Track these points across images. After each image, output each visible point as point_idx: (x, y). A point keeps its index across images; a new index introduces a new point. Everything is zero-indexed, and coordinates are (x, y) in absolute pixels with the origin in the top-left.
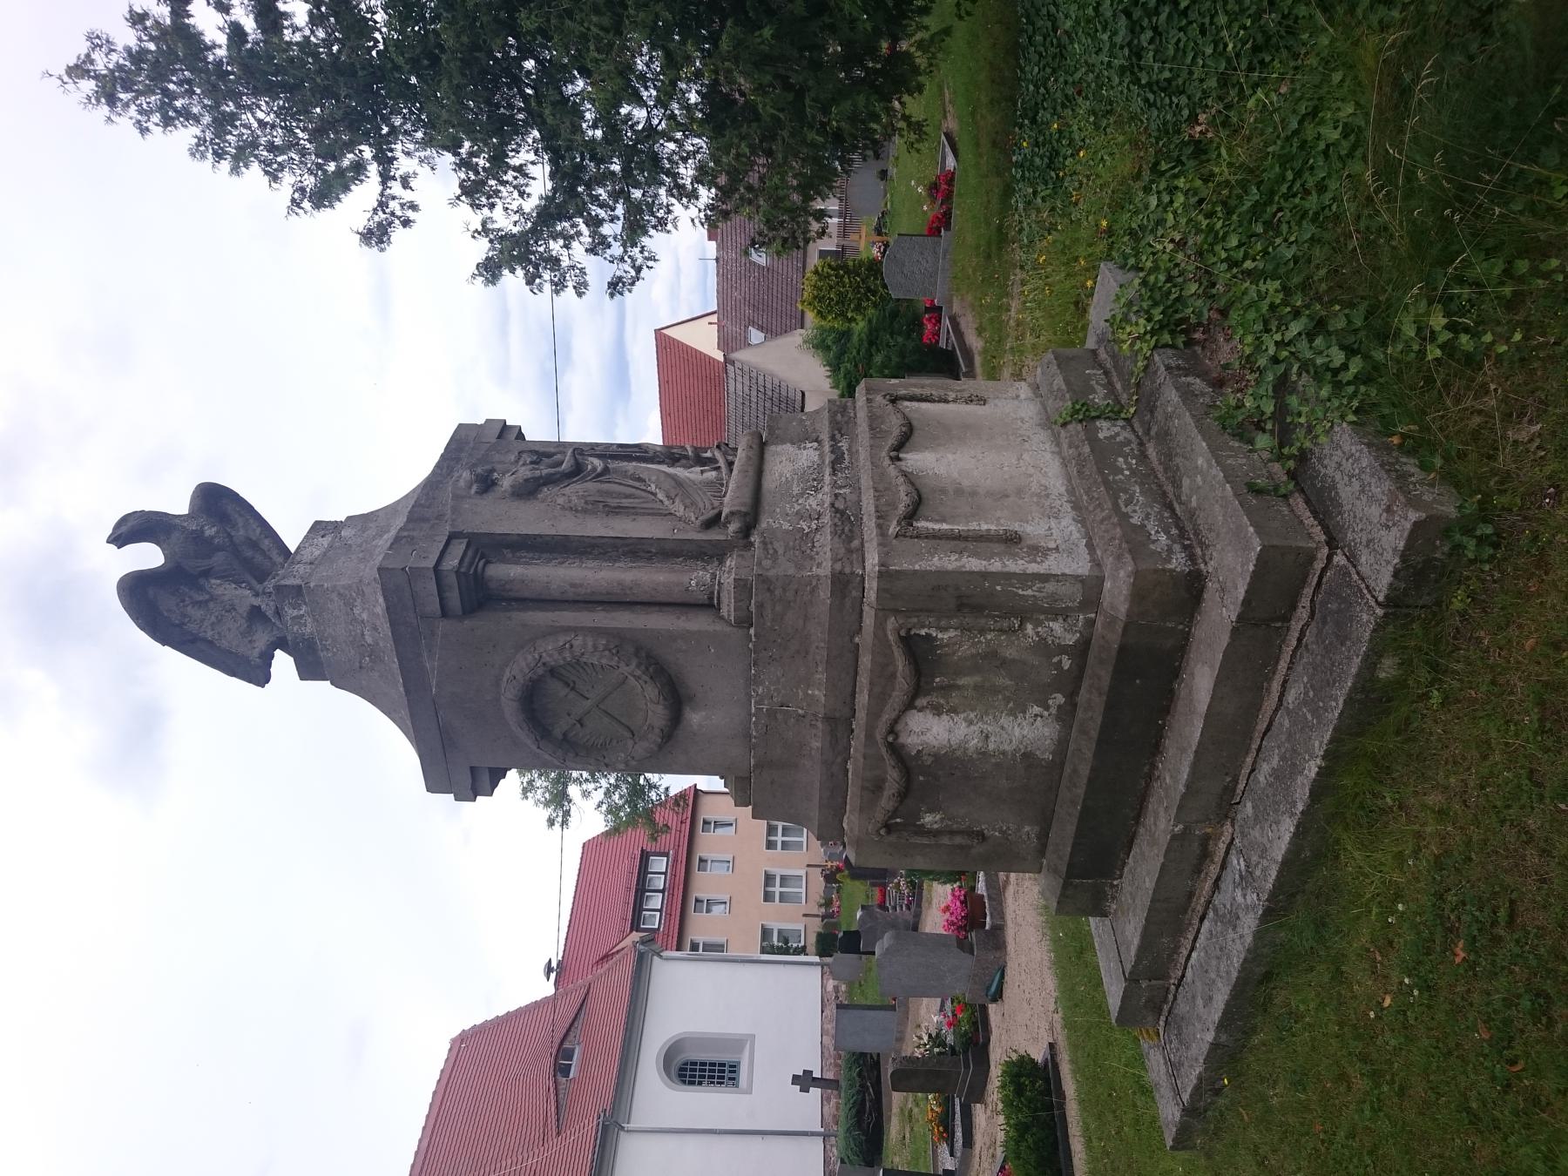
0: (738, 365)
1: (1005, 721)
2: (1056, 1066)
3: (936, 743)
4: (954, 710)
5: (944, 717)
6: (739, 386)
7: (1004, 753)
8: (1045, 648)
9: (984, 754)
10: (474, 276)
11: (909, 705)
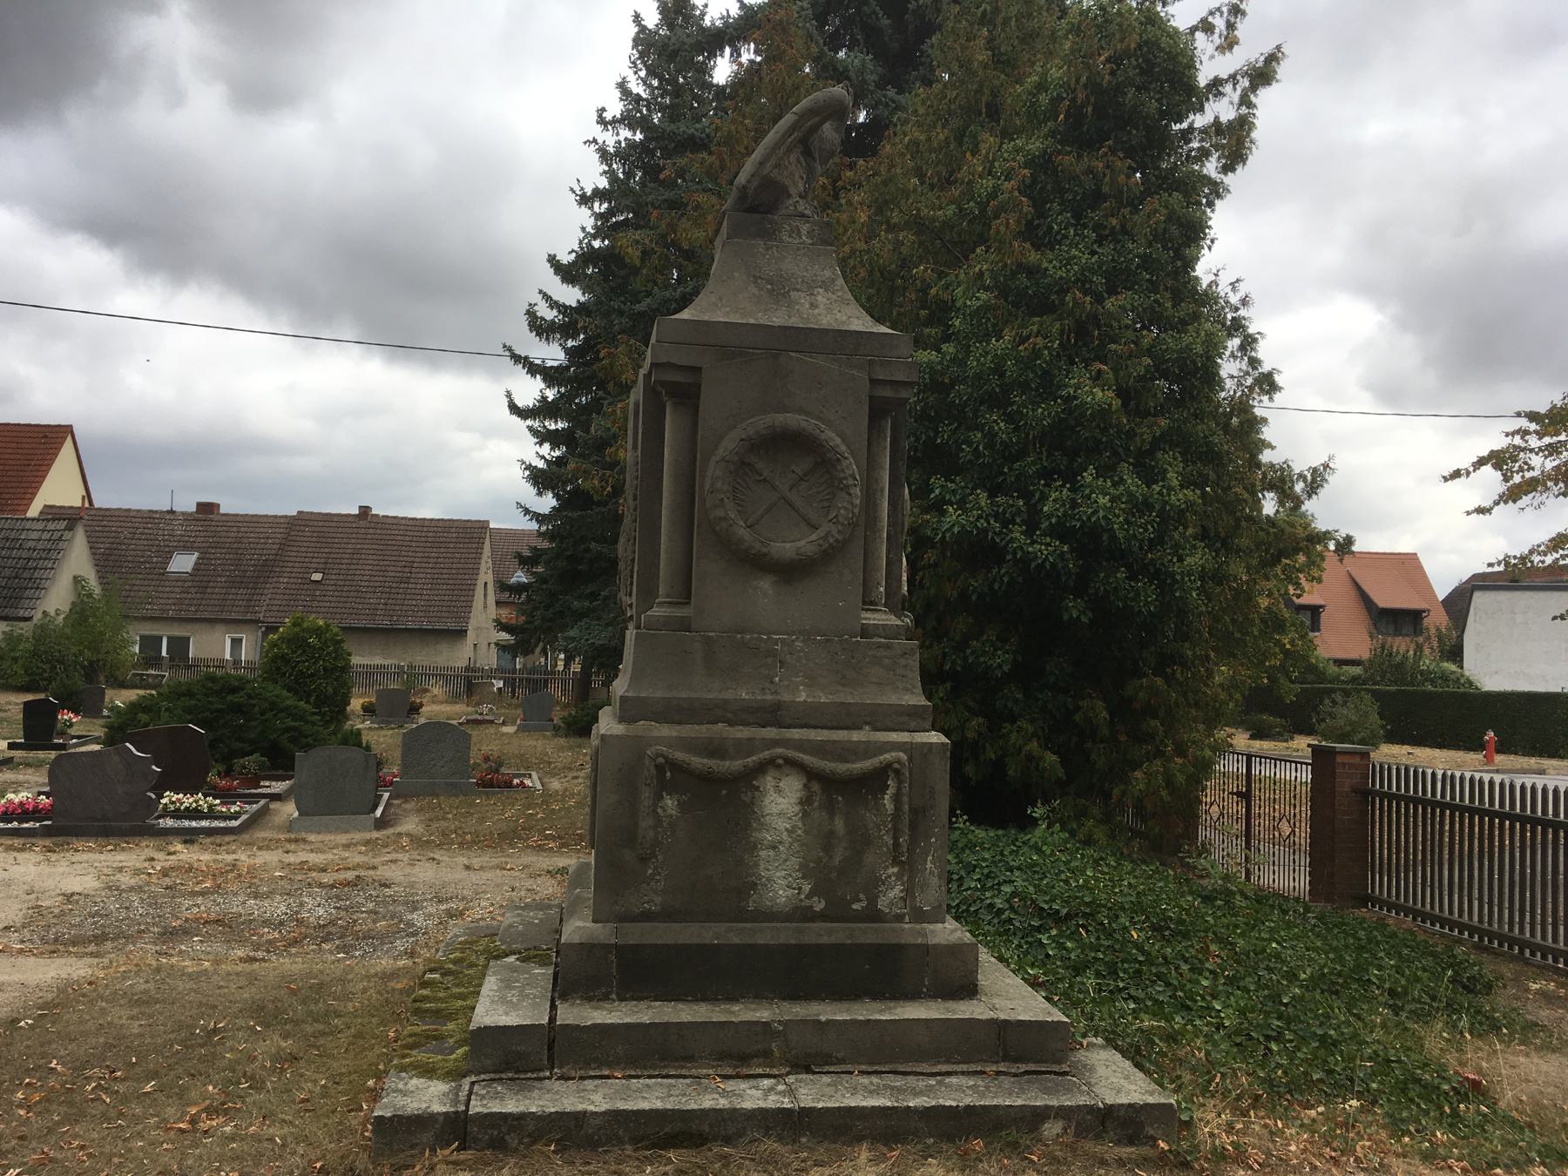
0: (67, 535)
1: (794, 862)
2: (742, 915)
3: (767, 802)
4: (805, 815)
5: (797, 808)
6: (34, 535)
7: (756, 865)
8: (874, 886)
9: (754, 848)
10: (1341, 561)
11: (810, 774)
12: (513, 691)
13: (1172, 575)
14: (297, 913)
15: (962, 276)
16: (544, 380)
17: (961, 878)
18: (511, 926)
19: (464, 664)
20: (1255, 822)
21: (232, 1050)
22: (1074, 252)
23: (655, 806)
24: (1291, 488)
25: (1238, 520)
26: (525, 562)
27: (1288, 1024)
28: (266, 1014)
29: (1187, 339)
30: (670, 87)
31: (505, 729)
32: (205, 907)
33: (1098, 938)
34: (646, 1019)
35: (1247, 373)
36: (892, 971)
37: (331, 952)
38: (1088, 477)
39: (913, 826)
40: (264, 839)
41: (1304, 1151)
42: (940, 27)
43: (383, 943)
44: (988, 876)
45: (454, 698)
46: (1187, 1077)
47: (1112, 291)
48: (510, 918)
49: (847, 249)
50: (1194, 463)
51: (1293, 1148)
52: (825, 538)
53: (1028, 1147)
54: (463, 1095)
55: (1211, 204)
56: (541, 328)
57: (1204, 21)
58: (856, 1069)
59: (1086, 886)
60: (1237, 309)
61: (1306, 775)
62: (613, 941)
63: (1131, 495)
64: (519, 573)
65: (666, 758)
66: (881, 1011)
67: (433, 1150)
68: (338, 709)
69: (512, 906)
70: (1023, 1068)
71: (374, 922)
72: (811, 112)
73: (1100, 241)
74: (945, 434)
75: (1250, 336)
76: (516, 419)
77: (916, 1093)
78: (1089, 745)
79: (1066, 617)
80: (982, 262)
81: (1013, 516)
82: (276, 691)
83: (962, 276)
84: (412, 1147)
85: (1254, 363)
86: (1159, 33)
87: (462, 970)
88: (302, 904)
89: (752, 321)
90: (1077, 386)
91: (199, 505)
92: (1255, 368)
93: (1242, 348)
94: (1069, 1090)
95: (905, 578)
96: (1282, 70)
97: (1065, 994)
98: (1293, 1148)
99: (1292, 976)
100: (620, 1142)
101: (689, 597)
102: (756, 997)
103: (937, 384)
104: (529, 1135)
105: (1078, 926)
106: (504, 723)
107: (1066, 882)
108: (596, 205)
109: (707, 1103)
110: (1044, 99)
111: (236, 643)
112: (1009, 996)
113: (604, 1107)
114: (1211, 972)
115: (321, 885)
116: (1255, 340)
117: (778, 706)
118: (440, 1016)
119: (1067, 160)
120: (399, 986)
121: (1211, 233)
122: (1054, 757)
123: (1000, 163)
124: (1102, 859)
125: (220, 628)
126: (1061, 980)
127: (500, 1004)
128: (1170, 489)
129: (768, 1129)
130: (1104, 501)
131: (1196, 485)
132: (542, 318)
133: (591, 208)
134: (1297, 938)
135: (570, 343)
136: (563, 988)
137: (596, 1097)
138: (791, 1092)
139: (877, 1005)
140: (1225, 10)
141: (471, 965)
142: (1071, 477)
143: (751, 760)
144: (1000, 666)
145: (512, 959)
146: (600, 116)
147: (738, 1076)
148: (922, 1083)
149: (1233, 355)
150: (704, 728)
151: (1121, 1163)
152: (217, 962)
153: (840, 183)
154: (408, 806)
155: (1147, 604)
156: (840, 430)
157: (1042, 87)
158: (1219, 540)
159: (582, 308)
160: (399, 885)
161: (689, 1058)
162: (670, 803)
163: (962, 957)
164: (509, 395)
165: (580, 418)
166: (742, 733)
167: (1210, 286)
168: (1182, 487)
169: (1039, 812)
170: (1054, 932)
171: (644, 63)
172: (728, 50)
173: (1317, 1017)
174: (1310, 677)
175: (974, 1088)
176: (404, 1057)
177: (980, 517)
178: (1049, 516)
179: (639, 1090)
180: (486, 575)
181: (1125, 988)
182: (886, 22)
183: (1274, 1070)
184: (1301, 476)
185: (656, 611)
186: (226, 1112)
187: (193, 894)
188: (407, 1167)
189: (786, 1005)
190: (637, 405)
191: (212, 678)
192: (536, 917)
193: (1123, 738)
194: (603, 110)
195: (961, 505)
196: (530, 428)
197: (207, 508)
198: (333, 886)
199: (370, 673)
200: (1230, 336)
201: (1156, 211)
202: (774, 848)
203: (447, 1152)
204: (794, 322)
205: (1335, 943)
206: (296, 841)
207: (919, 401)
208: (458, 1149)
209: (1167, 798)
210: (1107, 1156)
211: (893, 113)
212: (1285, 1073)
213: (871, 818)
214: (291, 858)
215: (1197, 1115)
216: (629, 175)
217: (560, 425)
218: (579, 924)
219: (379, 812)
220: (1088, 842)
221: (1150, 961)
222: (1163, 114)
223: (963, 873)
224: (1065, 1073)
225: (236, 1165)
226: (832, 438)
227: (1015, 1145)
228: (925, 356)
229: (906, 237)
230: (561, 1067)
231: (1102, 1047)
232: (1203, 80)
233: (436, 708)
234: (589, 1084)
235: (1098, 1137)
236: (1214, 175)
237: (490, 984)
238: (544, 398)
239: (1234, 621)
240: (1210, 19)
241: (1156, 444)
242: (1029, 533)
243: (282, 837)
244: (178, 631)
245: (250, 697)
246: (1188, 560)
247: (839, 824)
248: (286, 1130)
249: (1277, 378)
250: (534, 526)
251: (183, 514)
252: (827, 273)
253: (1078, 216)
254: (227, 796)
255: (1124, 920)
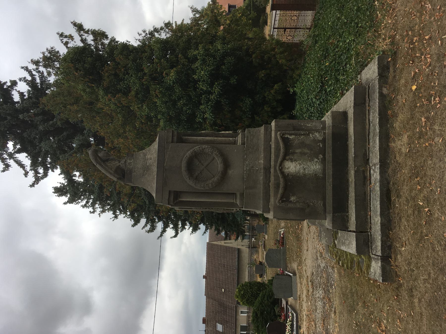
1: (309, 163)
2: (324, 178)
3: (292, 171)
4: (296, 160)
5: (294, 163)
7: (310, 174)
8: (315, 141)
9: (305, 175)
11: (284, 159)
12: (255, 235)
13: (223, 52)
14: (321, 299)
15: (139, 113)
16: (167, 228)
17: (311, 113)
18: (326, 241)
19: (248, 249)
20: (292, 26)
21: (362, 319)
22: (131, 81)
23: (293, 203)
24: (197, 18)
25: (207, 33)
26: (219, 233)
27: (353, 21)
28: (351, 310)
29: (156, 49)
30: (84, 193)
31: (266, 238)
32: (319, 324)
33: (328, 74)
34: (354, 206)
35: (165, 30)
36: (339, 136)
37: (333, 290)
38: (196, 77)
39: (298, 130)
40: (299, 306)
41: (391, 18)
42: (68, 119)
43: (330, 275)
44: (310, 105)
45: (257, 252)
46: (369, 51)
47: (142, 70)
48: (324, 241)
49: (131, 145)
50: (191, 46)
51: (390, 21)
52: (217, 155)
53: (390, 98)
54: (376, 257)
55: (117, 42)
56: (153, 229)
57: (65, 44)
58: (368, 146)
59: (313, 77)
60: (147, 34)
61: (278, 12)
62: (332, 214)
63: (201, 64)
64: (222, 234)
65: (280, 200)
66: (351, 139)
67: (391, 266)
68: (261, 285)
69: (320, 241)
70: (367, 99)
71: (324, 277)
72: (96, 160)
73: (128, 74)
74: (184, 118)
75: (154, 30)
76: (178, 236)
77: (375, 129)
78: (272, 76)
79: (236, 83)
80: (134, 107)
81: (207, 98)
82: (257, 303)
83: (139, 113)
84: (390, 271)
85: (162, 29)
86: (68, 57)
87: (340, 256)
88: (318, 297)
89: (156, 176)
90: (170, 80)
91: (203, 323)
92: (163, 28)
93: (157, 32)
94: (374, 86)
95: (227, 132)
96: (78, 22)
97: (345, 85)
98: (390, 21)
99: (339, 19)
100: (389, 213)
101: (234, 193)
102: (347, 174)
103: (169, 120)
104: (387, 239)
105: (325, 80)
106: (265, 238)
107: (312, 83)
108: (117, 214)
109: (378, 189)
110: (88, 90)
111: (242, 312)
112: (347, 102)
113: (379, 218)
114: (338, 42)
115: (313, 292)
116: (155, 28)
117: (265, 168)
118: (352, 262)
119: (105, 83)
120: (343, 272)
121: (125, 42)
122: (276, 86)
123: (106, 102)
124: (305, 72)
125: (238, 316)
126: (341, 86)
127: (350, 247)
128: (199, 53)
129: (385, 172)
130: (203, 73)
131: (198, 46)
132: (150, 228)
133: (118, 215)
134: (327, 16)
135: (157, 221)
136: (345, 228)
137: (376, 220)
138: (375, 165)
139: (349, 139)
140: (61, 38)
141: (337, 252)
142: (196, 82)
143: (280, 176)
144: (250, 101)
145: (336, 242)
146: (92, 213)
147: (370, 179)
148: (372, 128)
149: (160, 35)
150: (271, 189)
151: (395, 71)
152: (336, 322)
153: (112, 147)
154: (289, 266)
155: (232, 60)
156: (187, 151)
157: (84, 91)
158: (213, 39)
159: (147, 218)
160: (313, 270)
161: (365, 193)
162: (292, 199)
163: (335, 115)
164: (171, 238)
165: (178, 217)
166: (272, 179)
167: (140, 41)
168: (198, 50)
169: (292, 91)
170: (327, 87)
171: (77, 200)
172: (74, 178)
173: (351, 12)
174: (249, 8)
175: (373, 113)
176: (364, 273)
177: (207, 108)
178: (207, 88)
179: (374, 208)
180: (222, 243)
181: (343, 67)
182: (65, 133)
183: (367, 26)
184: (194, 15)
185: (238, 202)
186: (380, 322)
187: (316, 327)
188: (396, 273)
189: (349, 166)
190: (180, 208)
191: (253, 320)
192: (323, 234)
193: (270, 66)
194: (90, 212)
195: (204, 113)
196: (181, 231)
197: (204, 321)
198: (313, 288)
199: (251, 275)
200: (154, 35)
201: (120, 58)
202: (305, 169)
203: (392, 262)
204: (155, 164)
205: (329, 5)
206: (300, 298)
207: (174, 125)
208: (391, 259)
209: (287, 53)
210: (393, 75)
211: (91, 131)
212: (367, 22)
213: (296, 142)
214: (305, 299)
215: (381, 49)
216: (109, 204)
217: (180, 223)
218: (327, 224)
219: (291, 275)
220: (300, 76)
221: (335, 59)
222: (92, 56)
223: (309, 112)
224: (369, 87)
225: (395, 320)
226: (189, 154)
227: (390, 102)
228: (162, 123)
229: (128, 128)
230: (368, 229)
231: (361, 75)
232: (81, 45)
233: (260, 257)
234: (372, 221)
235: (387, 78)
236: (108, 41)
237: (343, 248)
238: (172, 228)
239: (236, 34)
240: (64, 43)
241: (186, 57)
242: (212, 94)
243: (298, 302)
244: (239, 329)
245: (258, 310)
246: (219, 48)
247: (298, 151)
248: (386, 306)
249: (167, 22)
250: (208, 230)
251: (206, 327)
252: (142, 155)
253: (121, 80)
254: (287, 317)
255: (323, 67)
